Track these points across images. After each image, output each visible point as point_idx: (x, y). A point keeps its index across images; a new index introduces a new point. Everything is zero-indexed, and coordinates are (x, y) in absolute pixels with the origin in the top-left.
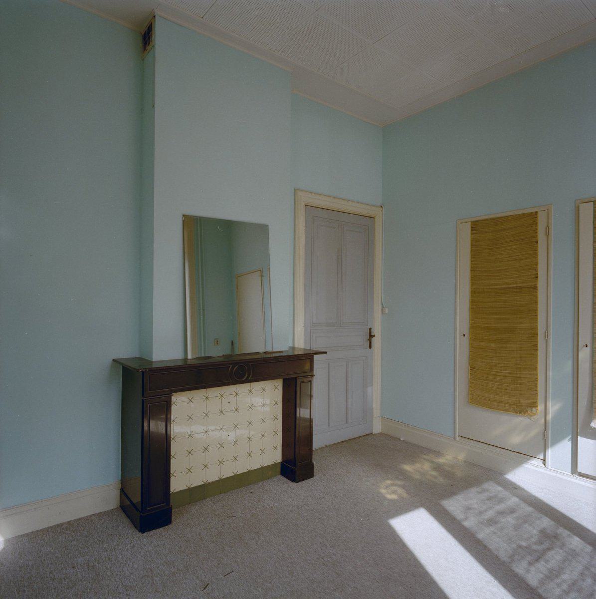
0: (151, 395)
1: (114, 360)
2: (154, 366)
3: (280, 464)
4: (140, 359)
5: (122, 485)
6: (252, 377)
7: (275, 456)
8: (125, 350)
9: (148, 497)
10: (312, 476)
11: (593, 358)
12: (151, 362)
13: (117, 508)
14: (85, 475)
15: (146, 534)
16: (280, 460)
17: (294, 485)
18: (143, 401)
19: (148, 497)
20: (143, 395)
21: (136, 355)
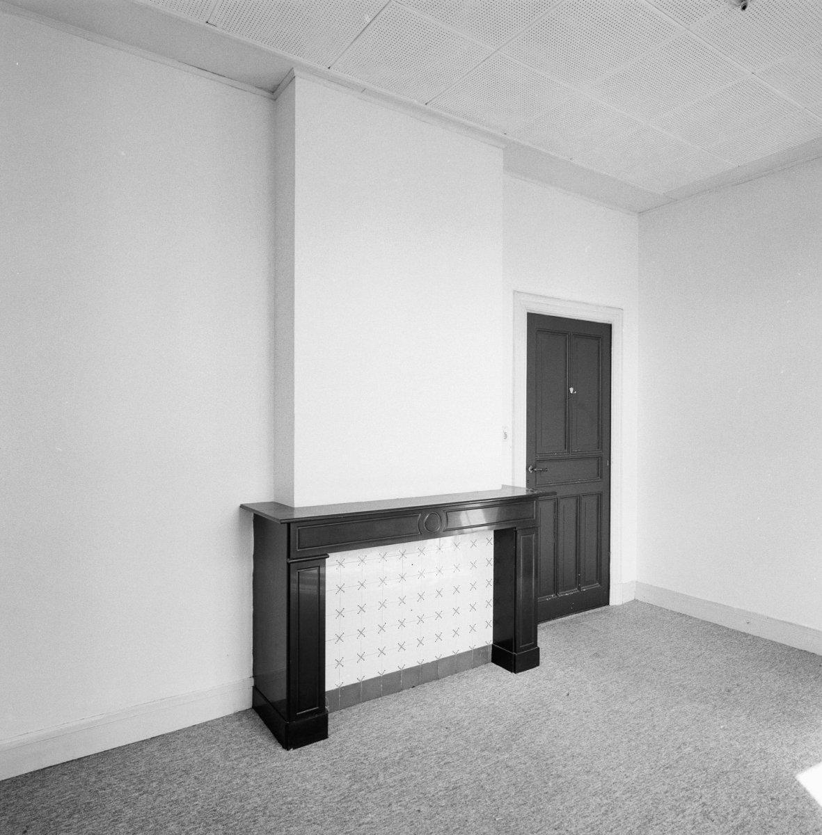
0: (311, 555)
1: (242, 506)
2: (297, 515)
3: (490, 650)
4: (278, 506)
5: (255, 682)
6: (532, 537)
7: (485, 637)
8: (258, 493)
9: (292, 700)
10: (538, 665)
11: (537, 538)
12: (292, 509)
13: (239, 715)
14: (203, 668)
15: (292, 751)
16: (492, 643)
17: (280, 751)
18: (289, 565)
19: (292, 700)
20: (289, 556)
21: (271, 499)
